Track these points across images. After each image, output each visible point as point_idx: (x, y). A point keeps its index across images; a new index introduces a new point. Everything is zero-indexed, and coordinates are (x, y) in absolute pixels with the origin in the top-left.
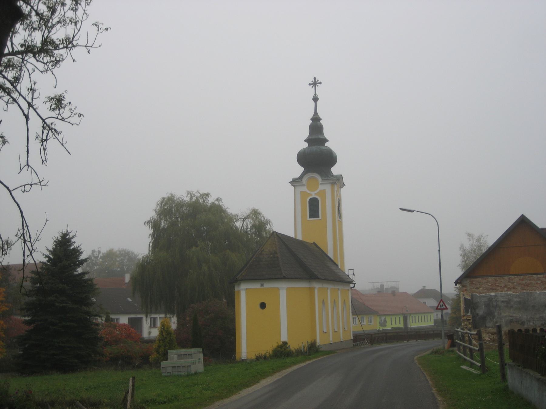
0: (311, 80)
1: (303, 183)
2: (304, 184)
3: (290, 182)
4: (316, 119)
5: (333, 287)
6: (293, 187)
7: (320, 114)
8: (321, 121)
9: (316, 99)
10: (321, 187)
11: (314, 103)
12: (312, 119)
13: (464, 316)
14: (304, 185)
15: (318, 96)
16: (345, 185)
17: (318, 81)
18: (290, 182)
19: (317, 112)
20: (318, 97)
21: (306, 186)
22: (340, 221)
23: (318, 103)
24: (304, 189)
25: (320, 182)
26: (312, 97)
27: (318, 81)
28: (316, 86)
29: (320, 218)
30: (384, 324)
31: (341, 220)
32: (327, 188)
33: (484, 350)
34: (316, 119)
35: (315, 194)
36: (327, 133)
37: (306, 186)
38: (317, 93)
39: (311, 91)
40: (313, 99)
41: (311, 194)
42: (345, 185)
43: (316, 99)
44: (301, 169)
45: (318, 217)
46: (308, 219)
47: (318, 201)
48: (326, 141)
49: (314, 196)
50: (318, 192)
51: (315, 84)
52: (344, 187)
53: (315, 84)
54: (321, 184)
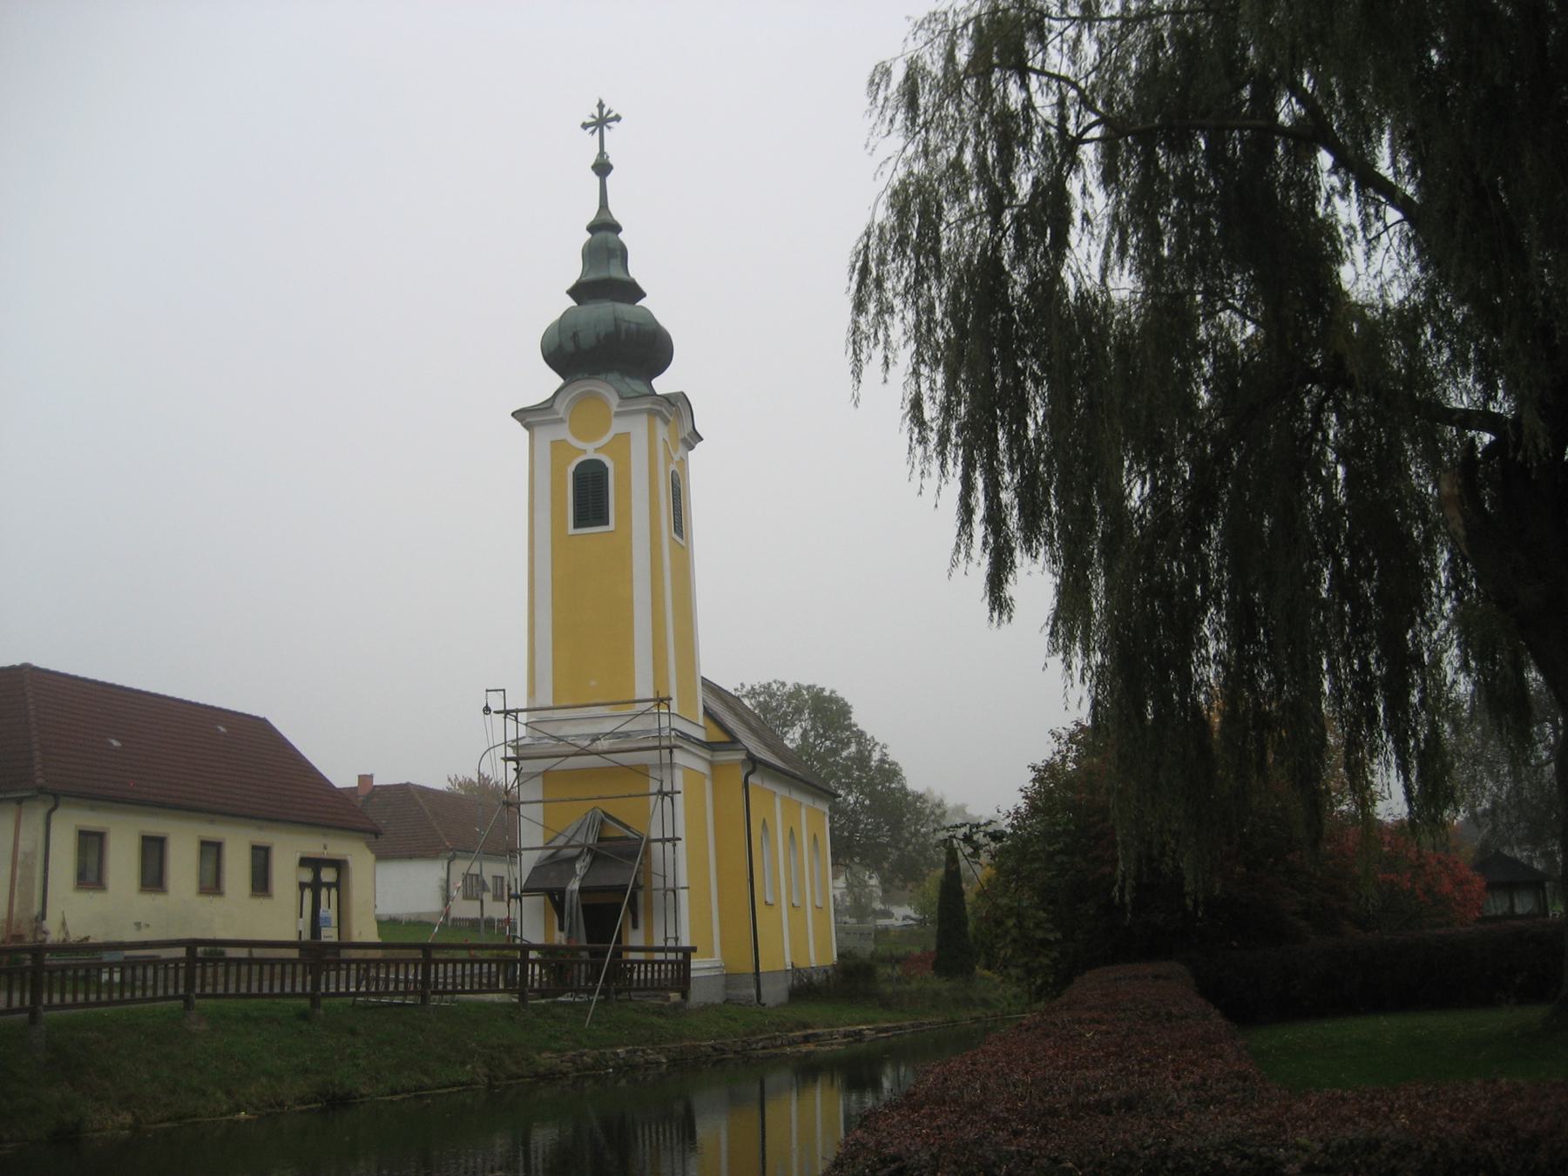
0: (589, 112)
1: (557, 413)
2: (560, 416)
3: (521, 415)
4: (604, 227)
5: (787, 794)
6: (526, 433)
7: (617, 213)
8: (621, 236)
9: (602, 168)
10: (618, 426)
11: (597, 180)
12: (592, 228)
13: (1500, 789)
14: (561, 421)
15: (610, 159)
16: (702, 439)
17: (609, 112)
18: (521, 415)
19: (607, 206)
20: (611, 161)
21: (566, 425)
22: (683, 547)
23: (609, 179)
24: (563, 433)
25: (614, 409)
26: (592, 162)
27: (609, 112)
28: (605, 128)
29: (612, 526)
30: (250, 952)
31: (687, 543)
32: (638, 429)
33: (944, 858)
34: (604, 227)
35: (596, 450)
36: (638, 271)
37: (566, 425)
38: (606, 150)
39: (588, 147)
40: (594, 167)
41: (585, 451)
42: (702, 439)
43: (602, 168)
44: (556, 381)
45: (607, 523)
46: (571, 530)
47: (607, 469)
48: (642, 295)
49: (591, 455)
50: (607, 444)
51: (601, 122)
52: (699, 446)
53: (601, 122)
54: (617, 414)
